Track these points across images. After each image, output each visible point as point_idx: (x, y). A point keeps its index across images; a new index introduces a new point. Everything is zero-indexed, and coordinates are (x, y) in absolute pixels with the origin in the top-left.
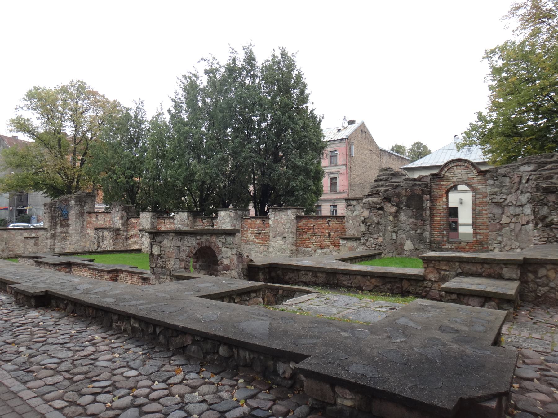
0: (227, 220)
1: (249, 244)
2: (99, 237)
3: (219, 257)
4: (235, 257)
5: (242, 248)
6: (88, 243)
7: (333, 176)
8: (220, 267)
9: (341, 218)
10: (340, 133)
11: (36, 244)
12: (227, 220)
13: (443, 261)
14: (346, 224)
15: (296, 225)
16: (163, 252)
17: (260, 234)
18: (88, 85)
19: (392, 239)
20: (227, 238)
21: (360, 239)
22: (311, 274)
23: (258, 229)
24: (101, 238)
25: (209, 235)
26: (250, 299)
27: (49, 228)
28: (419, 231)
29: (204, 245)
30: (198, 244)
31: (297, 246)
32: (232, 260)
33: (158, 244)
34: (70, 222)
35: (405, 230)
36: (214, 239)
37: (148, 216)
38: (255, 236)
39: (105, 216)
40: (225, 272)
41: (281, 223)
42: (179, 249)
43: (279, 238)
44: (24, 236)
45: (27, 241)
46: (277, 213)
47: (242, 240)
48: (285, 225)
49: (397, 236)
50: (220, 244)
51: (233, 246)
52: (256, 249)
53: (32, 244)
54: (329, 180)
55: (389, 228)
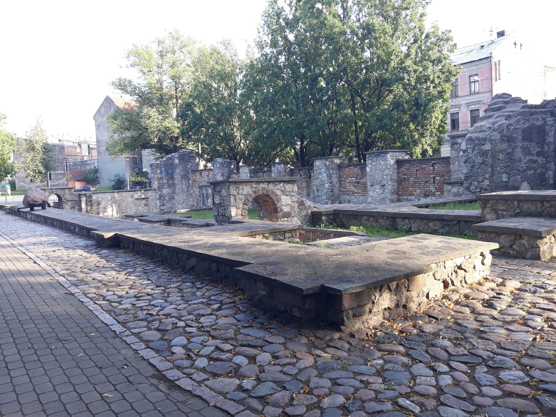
0: (323, 170)
1: (348, 195)
2: (203, 196)
3: (278, 205)
4: (296, 205)
5: (341, 199)
6: (195, 202)
7: (473, 107)
8: (281, 214)
9: (447, 160)
10: (485, 50)
11: (146, 205)
12: (323, 170)
13: (501, 200)
14: (452, 166)
15: (396, 171)
16: (222, 201)
17: (358, 183)
18: (10, 132)
19: (502, 181)
20: (286, 186)
21: (462, 184)
22: (372, 219)
23: (357, 178)
24: (205, 195)
25: (266, 184)
26: (285, 238)
27: (157, 189)
28: (538, 171)
29: (261, 193)
30: (255, 192)
31: (398, 195)
32: (292, 207)
33: (218, 193)
34: (176, 182)
35: (519, 170)
36: (271, 186)
37: (247, 171)
38: (354, 186)
39: (208, 173)
40: (286, 219)
41: (380, 169)
42: (235, 198)
43: (378, 187)
44: (135, 198)
45: (138, 202)
46: (375, 159)
47: (340, 191)
48: (383, 171)
49: (509, 178)
50: (279, 193)
51: (293, 194)
52: (355, 200)
53: (143, 205)
54: (469, 113)
55: (498, 169)
